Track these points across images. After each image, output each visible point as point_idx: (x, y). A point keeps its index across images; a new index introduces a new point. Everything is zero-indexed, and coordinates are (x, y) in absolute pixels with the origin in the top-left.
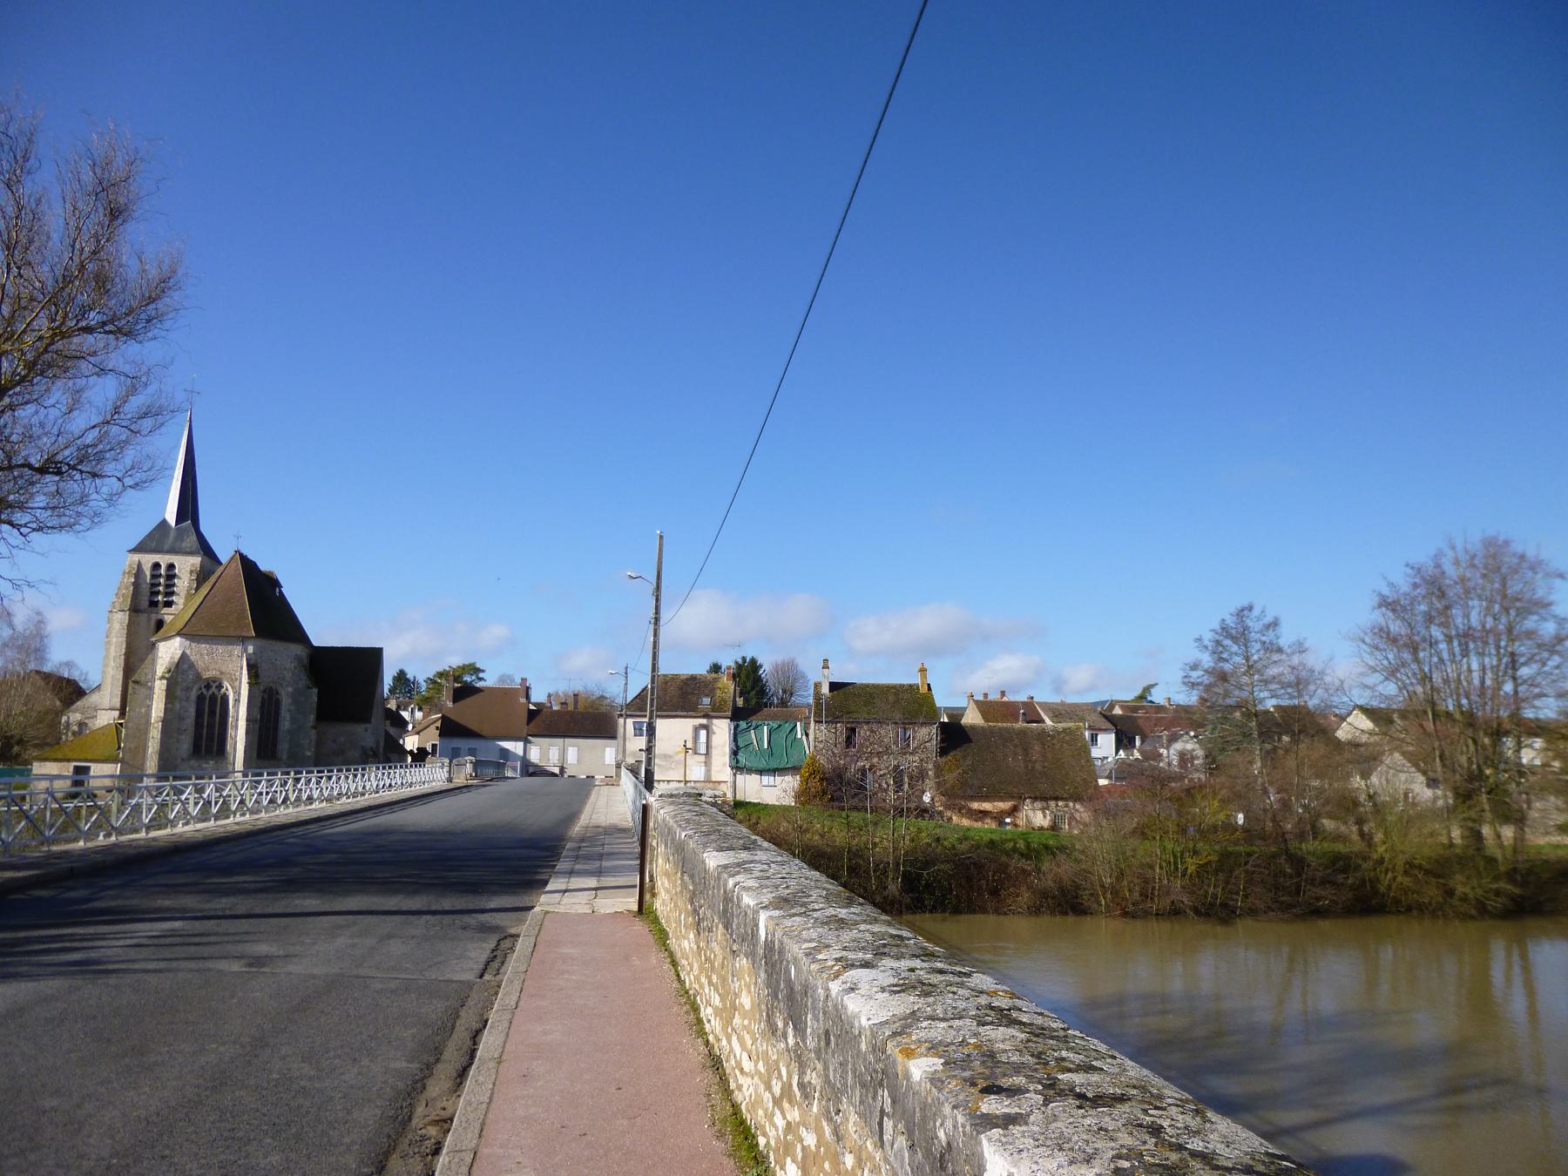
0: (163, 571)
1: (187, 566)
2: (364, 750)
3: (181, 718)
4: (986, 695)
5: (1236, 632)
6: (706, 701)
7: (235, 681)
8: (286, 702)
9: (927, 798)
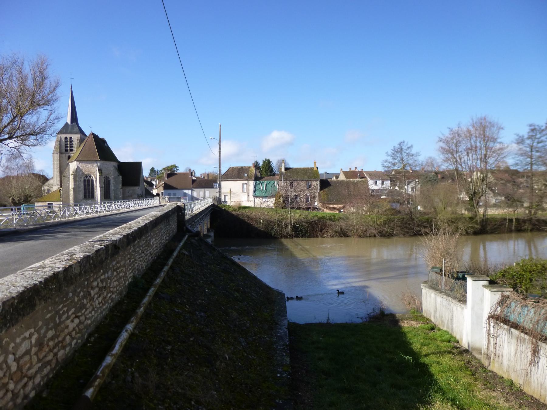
0: (68, 140)
1: (76, 137)
3: (79, 187)
5: (399, 150)
6: (246, 175)
9: (316, 204)
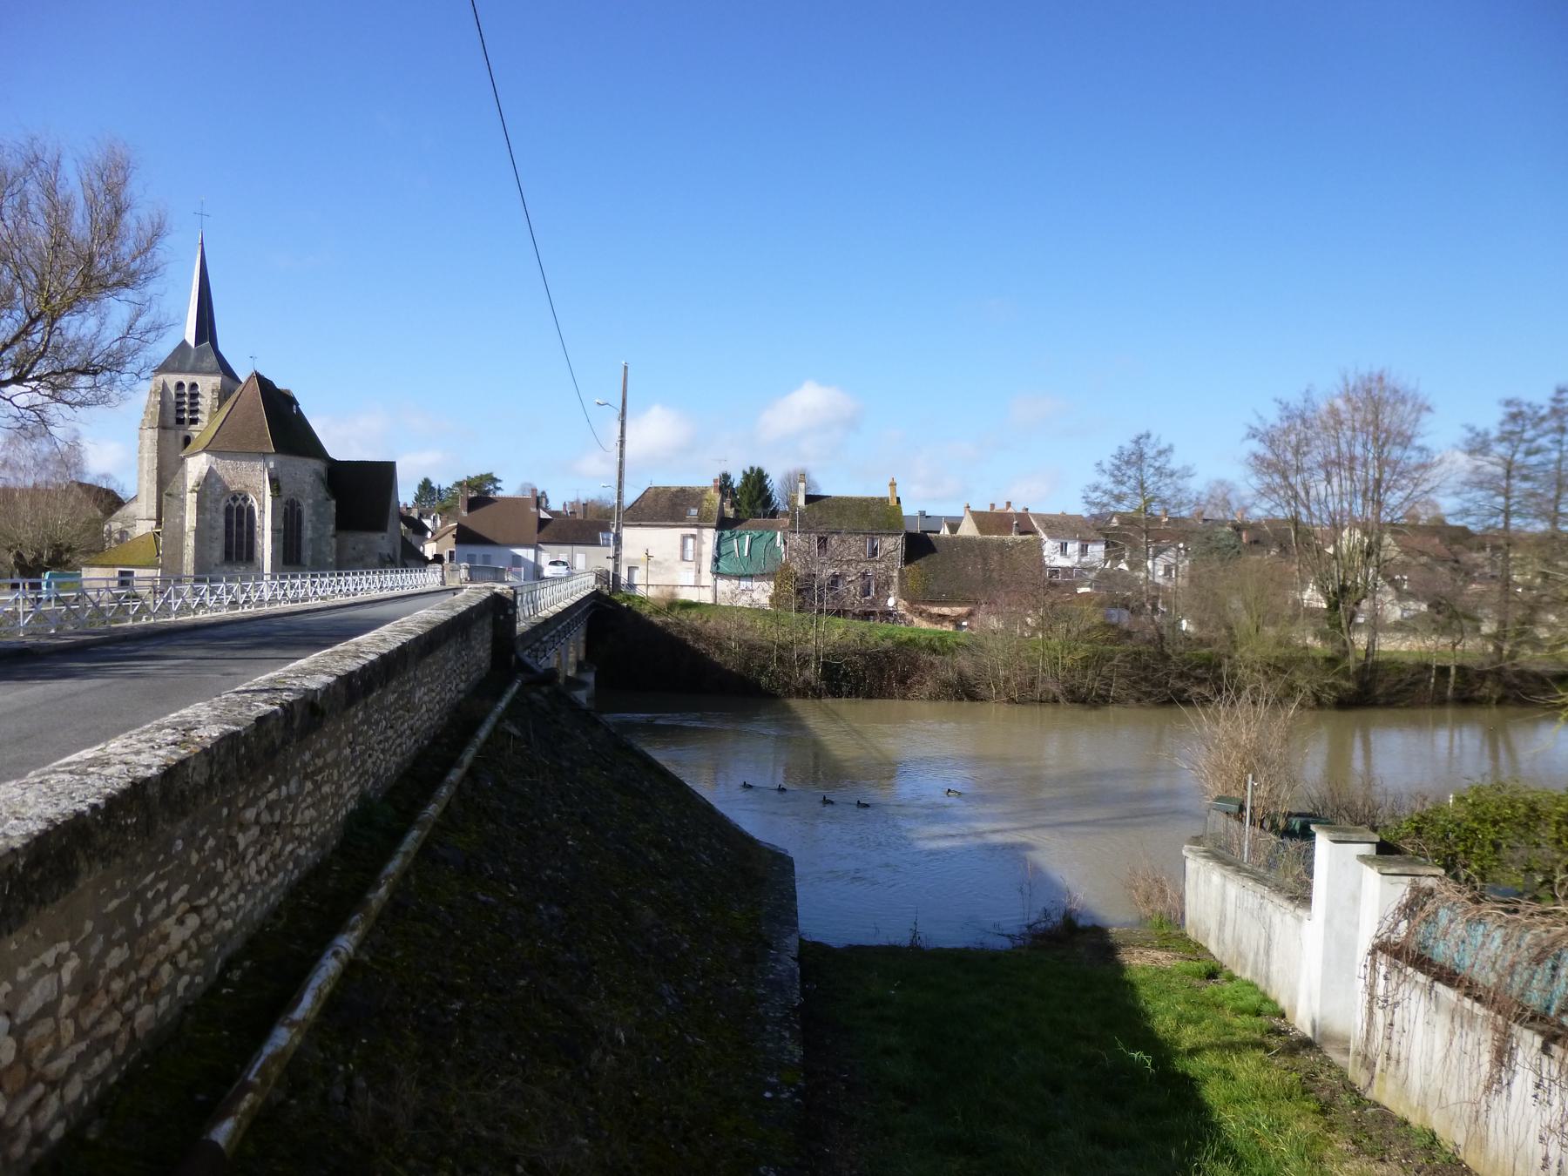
0: (186, 390)
1: (208, 385)
4: (993, 506)
5: (1134, 458)
6: (694, 511)
8: (307, 513)
9: (891, 602)
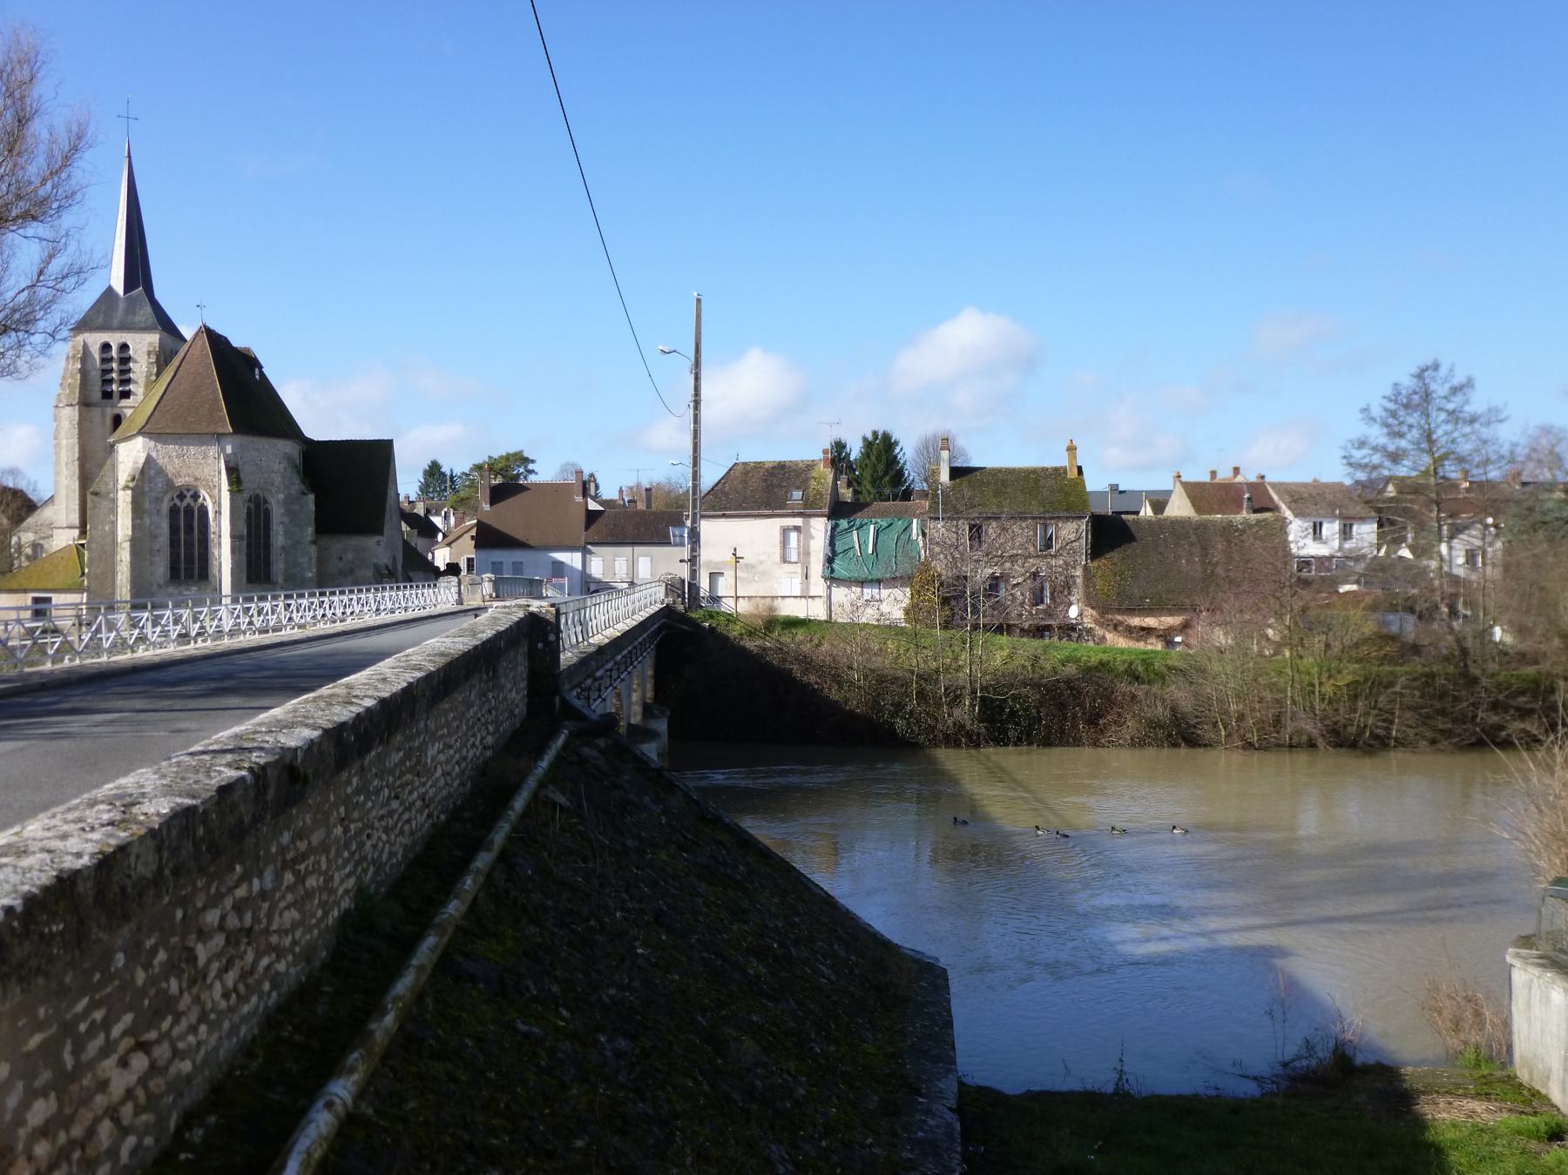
0: (114, 353)
1: (143, 345)
2: (377, 568)
3: (154, 537)
4: (1213, 474)
5: (1416, 400)
6: (797, 495)
7: (213, 488)
9: (1073, 612)
